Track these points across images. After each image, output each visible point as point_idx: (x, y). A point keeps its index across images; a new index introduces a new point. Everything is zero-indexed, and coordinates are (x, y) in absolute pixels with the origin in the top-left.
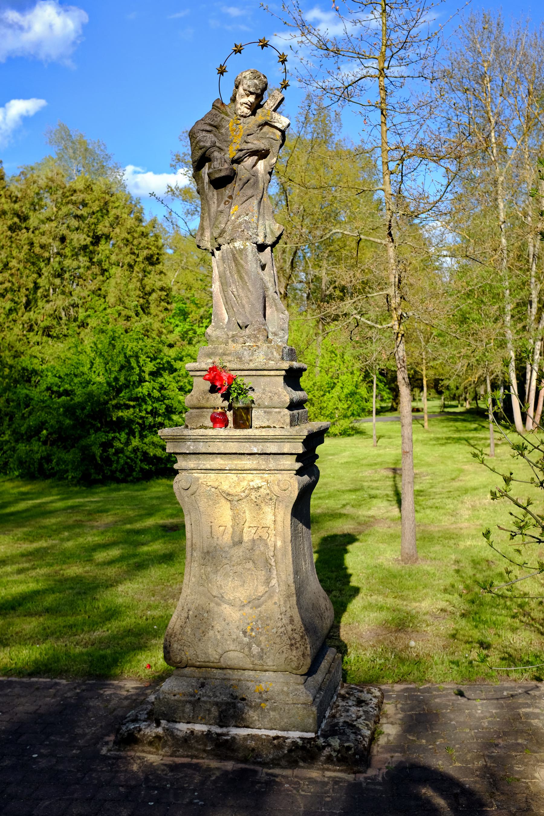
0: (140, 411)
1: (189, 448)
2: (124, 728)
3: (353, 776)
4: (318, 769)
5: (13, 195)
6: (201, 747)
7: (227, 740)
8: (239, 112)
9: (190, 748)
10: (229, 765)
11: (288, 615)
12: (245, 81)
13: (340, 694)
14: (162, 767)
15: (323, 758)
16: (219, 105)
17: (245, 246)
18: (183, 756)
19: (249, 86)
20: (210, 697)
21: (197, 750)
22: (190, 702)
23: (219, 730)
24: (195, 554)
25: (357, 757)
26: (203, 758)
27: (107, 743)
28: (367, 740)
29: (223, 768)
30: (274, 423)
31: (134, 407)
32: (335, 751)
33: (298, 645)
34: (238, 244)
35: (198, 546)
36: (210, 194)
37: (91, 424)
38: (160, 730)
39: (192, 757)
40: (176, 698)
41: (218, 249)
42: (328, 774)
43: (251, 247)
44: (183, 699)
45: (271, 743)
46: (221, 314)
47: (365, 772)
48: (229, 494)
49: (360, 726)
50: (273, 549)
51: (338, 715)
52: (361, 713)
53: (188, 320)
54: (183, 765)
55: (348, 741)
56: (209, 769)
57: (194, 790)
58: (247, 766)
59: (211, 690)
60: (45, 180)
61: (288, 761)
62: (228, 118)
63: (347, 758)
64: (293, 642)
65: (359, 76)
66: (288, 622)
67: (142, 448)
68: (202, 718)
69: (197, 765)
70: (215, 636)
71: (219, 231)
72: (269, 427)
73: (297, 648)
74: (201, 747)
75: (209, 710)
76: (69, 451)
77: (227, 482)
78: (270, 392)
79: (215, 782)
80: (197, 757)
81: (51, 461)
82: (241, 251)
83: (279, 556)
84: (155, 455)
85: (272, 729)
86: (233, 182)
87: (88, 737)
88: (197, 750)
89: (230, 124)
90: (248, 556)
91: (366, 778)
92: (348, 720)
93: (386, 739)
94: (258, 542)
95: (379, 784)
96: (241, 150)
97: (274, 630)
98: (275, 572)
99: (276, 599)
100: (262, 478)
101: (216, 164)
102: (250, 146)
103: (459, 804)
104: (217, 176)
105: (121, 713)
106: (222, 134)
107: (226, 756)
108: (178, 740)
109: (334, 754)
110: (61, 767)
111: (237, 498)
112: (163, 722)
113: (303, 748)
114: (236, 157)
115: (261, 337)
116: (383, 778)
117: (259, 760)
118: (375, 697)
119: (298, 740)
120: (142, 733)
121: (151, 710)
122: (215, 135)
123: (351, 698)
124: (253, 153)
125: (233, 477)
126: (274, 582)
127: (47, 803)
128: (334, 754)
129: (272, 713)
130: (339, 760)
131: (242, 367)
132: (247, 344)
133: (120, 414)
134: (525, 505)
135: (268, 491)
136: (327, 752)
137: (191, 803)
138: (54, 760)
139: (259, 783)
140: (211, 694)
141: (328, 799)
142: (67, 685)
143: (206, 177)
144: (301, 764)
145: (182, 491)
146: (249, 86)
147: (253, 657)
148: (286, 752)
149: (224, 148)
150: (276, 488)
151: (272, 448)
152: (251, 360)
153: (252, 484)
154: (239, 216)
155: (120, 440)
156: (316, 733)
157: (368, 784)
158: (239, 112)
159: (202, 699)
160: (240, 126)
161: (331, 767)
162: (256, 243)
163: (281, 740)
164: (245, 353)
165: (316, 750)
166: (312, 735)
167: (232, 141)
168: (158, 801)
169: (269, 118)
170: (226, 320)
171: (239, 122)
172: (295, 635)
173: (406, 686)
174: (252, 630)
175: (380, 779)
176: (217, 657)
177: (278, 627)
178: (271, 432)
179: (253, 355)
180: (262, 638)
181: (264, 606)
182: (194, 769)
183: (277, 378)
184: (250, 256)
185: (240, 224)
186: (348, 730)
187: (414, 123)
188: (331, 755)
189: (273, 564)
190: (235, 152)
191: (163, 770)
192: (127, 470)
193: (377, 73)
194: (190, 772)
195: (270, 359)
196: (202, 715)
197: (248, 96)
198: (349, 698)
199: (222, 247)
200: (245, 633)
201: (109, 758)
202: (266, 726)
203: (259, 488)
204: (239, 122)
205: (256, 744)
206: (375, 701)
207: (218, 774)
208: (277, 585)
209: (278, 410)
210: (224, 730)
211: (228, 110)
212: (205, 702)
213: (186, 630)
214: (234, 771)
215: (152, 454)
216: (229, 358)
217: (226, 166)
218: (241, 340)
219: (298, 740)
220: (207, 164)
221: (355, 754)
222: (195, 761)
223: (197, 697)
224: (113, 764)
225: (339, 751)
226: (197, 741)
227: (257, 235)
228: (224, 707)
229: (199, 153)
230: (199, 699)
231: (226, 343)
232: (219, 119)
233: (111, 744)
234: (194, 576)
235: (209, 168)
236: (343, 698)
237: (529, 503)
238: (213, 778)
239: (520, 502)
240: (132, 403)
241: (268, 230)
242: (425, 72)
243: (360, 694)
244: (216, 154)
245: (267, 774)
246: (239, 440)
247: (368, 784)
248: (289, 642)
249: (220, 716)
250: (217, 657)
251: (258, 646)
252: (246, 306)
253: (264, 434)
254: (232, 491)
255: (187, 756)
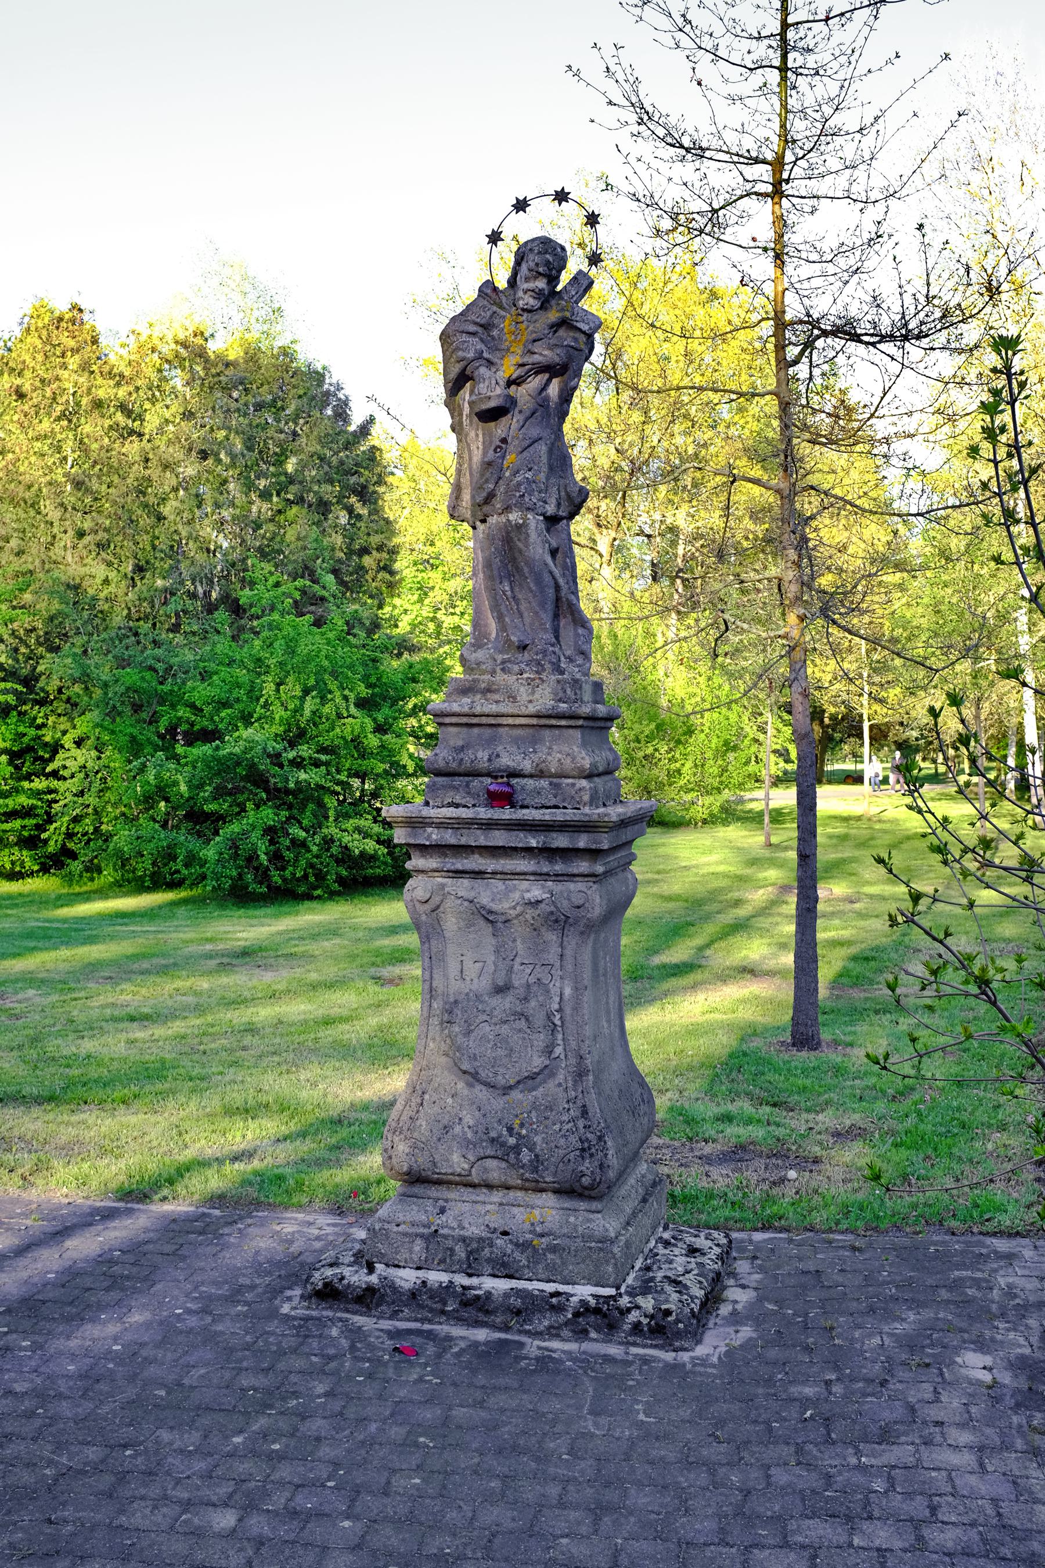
0: (338, 771)
1: (429, 837)
2: (317, 1275)
3: (673, 1354)
4: (620, 1343)
5: (115, 370)
6: (438, 1306)
7: (478, 1297)
8: (521, 303)
9: (422, 1307)
10: (481, 1335)
11: (579, 1103)
12: (531, 257)
13: (661, 1238)
14: (377, 1334)
15: (627, 1327)
16: (489, 291)
17: (525, 519)
18: (408, 1320)
19: (537, 265)
20: (453, 1229)
21: (431, 1310)
22: (422, 1236)
23: (466, 1281)
24: (435, 1005)
25: (681, 1326)
26: (440, 1323)
27: (289, 1299)
28: (698, 1301)
29: (472, 1338)
30: (564, 801)
31: (327, 764)
32: (646, 1316)
33: (593, 1150)
34: (514, 516)
35: (439, 992)
36: (472, 434)
37: (251, 792)
38: (374, 1279)
39: (422, 1321)
40: (400, 1229)
41: (483, 521)
42: (634, 1350)
43: (534, 521)
44: (411, 1230)
45: (547, 1303)
46: (486, 625)
47: (692, 1350)
48: (491, 912)
49: (689, 1283)
50: (558, 999)
51: (655, 1267)
52: (693, 1266)
53: (426, 602)
54: (409, 1332)
55: (667, 1301)
56: (449, 1338)
57: (426, 1365)
58: (509, 1337)
59: (455, 1218)
60: (173, 346)
61: (573, 1331)
62: (503, 313)
63: (664, 1327)
64: (586, 1145)
65: (739, 193)
66: (578, 1113)
67: (340, 840)
68: (441, 1262)
69: (430, 1332)
70: (464, 1133)
71: (485, 494)
72: (556, 807)
73: (592, 1155)
74: (438, 1306)
75: (452, 1250)
76: (208, 841)
77: (488, 893)
78: (560, 752)
79: (458, 1355)
80: (430, 1322)
81: (174, 858)
82: (519, 527)
83: (568, 1010)
84: (363, 854)
85: (549, 1281)
86: (509, 416)
87: (260, 1290)
88: (431, 1310)
89: (507, 323)
90: (518, 1009)
91: (692, 1358)
92: (669, 1274)
93: (730, 1308)
94: (535, 988)
95: (714, 1366)
96: (523, 365)
97: (557, 1127)
98: (560, 1036)
99: (560, 1077)
100: (543, 887)
101: (482, 388)
102: (537, 358)
103: (830, 1393)
104: (484, 407)
105: (310, 1260)
106: (493, 338)
107: (476, 1322)
108: (402, 1294)
109: (645, 1321)
110: (220, 1328)
111: (502, 918)
112: (379, 1267)
113: (597, 1311)
114: (514, 377)
115: (547, 666)
116: (720, 1358)
117: (527, 1327)
118: (718, 1245)
119: (590, 1299)
120: (345, 1282)
121: (360, 1251)
122: (482, 340)
123: (680, 1244)
124: (540, 369)
125: (498, 885)
126: (558, 1051)
127: (202, 1371)
128: (645, 1321)
129: (549, 1256)
130: (652, 1331)
131: (516, 712)
132: (525, 676)
133: (303, 776)
134: (942, 936)
135: (553, 908)
136: (633, 1316)
137: (421, 1380)
138: (209, 1319)
139: (526, 1358)
140: (455, 1224)
141: (631, 1383)
142: (222, 1217)
143: (466, 405)
144: (593, 1335)
145: (418, 905)
146: (537, 265)
147: (522, 1167)
148: (570, 1316)
149: (495, 360)
150: (565, 903)
151: (561, 841)
152: (530, 701)
153: (527, 896)
154: (518, 472)
155: (300, 823)
156: (618, 1288)
157: (695, 1365)
158: (521, 303)
159: (441, 1231)
160: (523, 326)
161: (639, 1340)
162: (543, 515)
163: (562, 1299)
164: (522, 689)
165: (616, 1313)
166: (612, 1291)
167: (508, 350)
168: (370, 1376)
169: (568, 314)
170: (494, 635)
171: (521, 319)
172: (589, 1135)
173: (772, 1235)
174: (522, 1125)
175: (715, 1359)
176: (466, 1166)
177: (562, 1123)
178: (559, 815)
179: (533, 693)
180: (538, 1139)
181: (541, 1089)
182: (427, 1338)
183: (571, 731)
184: (533, 536)
185: (519, 484)
186: (669, 1288)
187: (832, 279)
188: (640, 1322)
189: (558, 1023)
190: (513, 368)
191: (378, 1337)
192: (312, 879)
193: (769, 189)
194: (419, 1340)
195: (560, 700)
196: (440, 1256)
197: (536, 278)
198: (675, 1245)
199: (489, 519)
200: (510, 1130)
201: (294, 1318)
202: (540, 1276)
203: (538, 902)
204: (521, 319)
205: (523, 1303)
206: (717, 1250)
207: (463, 1344)
208: (562, 1057)
209: (570, 781)
210: (474, 1281)
211: (504, 300)
212: (445, 1237)
213: (418, 1123)
214: (487, 1343)
215: (357, 852)
216: (497, 697)
217: (498, 391)
218: (516, 668)
219: (590, 1299)
220: (468, 385)
221: (678, 1321)
222: (427, 1327)
223: (433, 1228)
224: (301, 1327)
225: (652, 1317)
226: (431, 1298)
227: (545, 502)
228: (475, 1245)
229: (456, 369)
230: (436, 1231)
231: (493, 673)
232: (489, 314)
233: (296, 1301)
234: (434, 1039)
235: (472, 392)
236: (667, 1244)
237: (947, 934)
238: (456, 1350)
239: (934, 933)
240: (324, 758)
241: (563, 494)
242: (855, 188)
243: (693, 1239)
244: (483, 370)
245: (539, 1348)
246: (489, 825)
247: (695, 1365)
248: (579, 1145)
249: (468, 1258)
250: (466, 1166)
251: (530, 1150)
252: (526, 614)
253: (547, 818)
254: (495, 907)
255: (416, 1320)
